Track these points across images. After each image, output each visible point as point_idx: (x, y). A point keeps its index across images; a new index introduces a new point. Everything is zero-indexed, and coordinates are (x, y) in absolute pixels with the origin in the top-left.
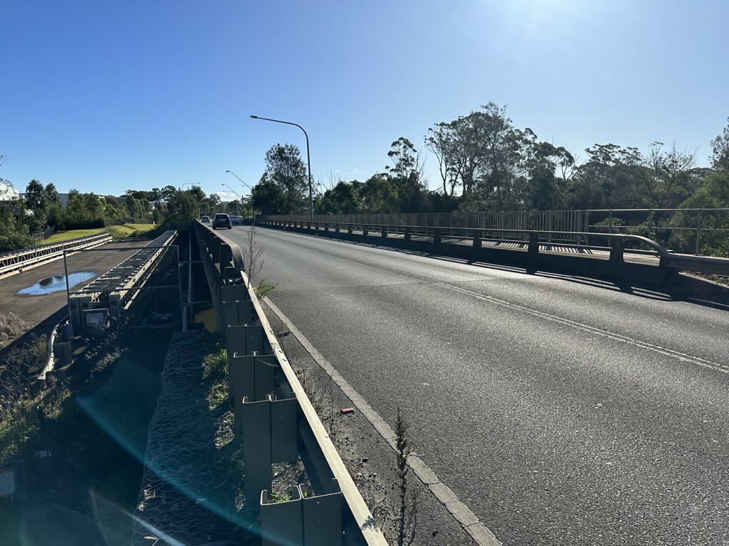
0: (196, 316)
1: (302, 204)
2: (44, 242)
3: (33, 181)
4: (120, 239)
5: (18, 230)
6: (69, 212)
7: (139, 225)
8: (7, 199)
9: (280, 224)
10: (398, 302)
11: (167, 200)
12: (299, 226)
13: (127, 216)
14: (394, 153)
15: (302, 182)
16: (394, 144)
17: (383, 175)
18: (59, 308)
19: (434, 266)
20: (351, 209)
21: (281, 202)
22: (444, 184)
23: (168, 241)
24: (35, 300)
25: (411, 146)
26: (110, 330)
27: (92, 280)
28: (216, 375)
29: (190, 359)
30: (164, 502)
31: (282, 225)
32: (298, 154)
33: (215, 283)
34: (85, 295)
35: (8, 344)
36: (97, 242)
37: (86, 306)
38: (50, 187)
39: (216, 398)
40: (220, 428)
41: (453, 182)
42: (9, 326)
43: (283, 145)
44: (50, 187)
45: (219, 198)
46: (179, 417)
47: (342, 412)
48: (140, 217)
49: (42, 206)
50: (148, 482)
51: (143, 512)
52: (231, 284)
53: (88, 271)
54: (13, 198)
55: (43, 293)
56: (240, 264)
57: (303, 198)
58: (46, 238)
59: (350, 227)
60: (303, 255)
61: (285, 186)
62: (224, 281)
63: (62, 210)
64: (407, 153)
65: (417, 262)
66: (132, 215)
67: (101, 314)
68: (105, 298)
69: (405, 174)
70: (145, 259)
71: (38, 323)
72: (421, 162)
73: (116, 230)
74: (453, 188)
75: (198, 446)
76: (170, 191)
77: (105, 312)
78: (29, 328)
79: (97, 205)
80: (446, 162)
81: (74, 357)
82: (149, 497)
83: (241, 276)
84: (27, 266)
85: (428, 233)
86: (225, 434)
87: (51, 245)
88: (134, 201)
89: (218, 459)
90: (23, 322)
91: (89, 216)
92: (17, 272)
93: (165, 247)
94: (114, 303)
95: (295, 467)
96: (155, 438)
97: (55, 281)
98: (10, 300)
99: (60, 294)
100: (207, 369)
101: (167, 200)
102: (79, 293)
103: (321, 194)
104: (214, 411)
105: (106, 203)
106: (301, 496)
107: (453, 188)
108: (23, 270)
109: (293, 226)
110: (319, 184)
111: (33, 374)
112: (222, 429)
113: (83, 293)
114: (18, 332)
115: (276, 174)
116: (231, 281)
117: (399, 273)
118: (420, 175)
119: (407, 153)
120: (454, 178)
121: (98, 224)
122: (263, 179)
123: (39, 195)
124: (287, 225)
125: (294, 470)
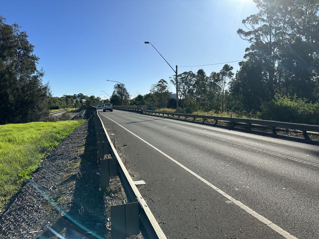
20: (143, 103)
25: (165, 82)
45: (100, 98)
66: (67, 105)
76: (81, 96)
106: (125, 203)
109: (130, 109)
121: (57, 108)
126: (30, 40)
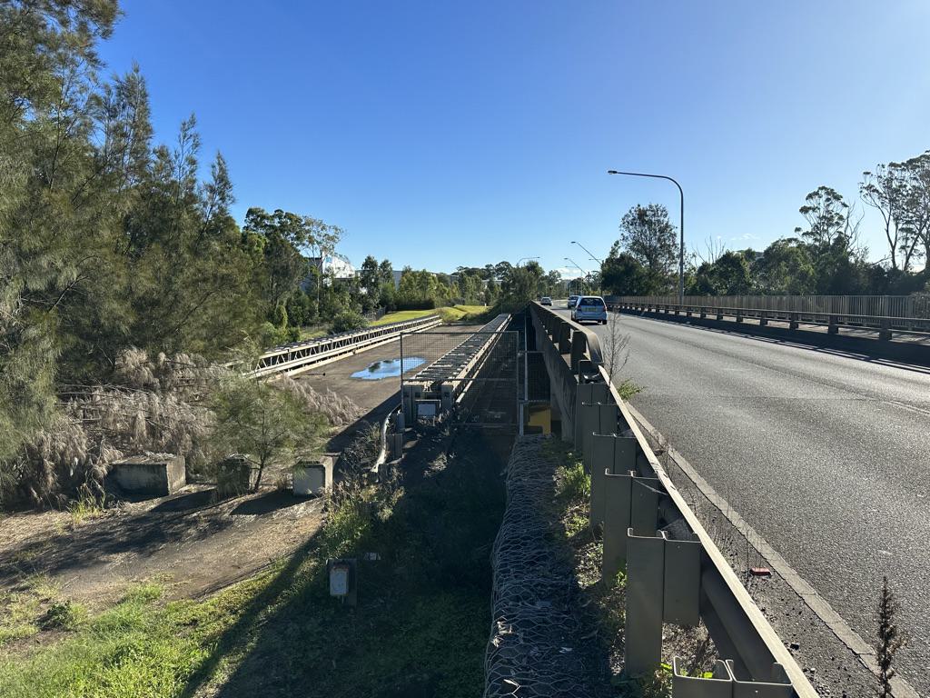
0: (531, 418)
1: (668, 282)
2: (376, 323)
3: (369, 258)
4: (450, 323)
5: (352, 307)
6: (401, 290)
7: (470, 307)
8: (344, 276)
9: (636, 308)
10: (827, 425)
11: (501, 278)
12: (663, 311)
13: (458, 296)
14: (810, 208)
15: (669, 252)
16: (810, 196)
17: (790, 240)
18: (390, 395)
19: (881, 375)
20: (741, 288)
21: (639, 279)
22: (893, 253)
23: (501, 326)
24: (366, 385)
25: (838, 198)
26: (441, 426)
27: (422, 367)
28: (572, 493)
29: (538, 470)
30: (522, 642)
31: (640, 309)
32: (666, 216)
33: (562, 379)
34: (418, 383)
35: (343, 429)
36: (427, 325)
37: (418, 396)
38: (385, 264)
39: (574, 523)
40: (582, 562)
41: (909, 250)
42: (344, 411)
43: (644, 206)
44: (385, 264)
45: (559, 275)
46: (529, 538)
47: (751, 571)
48: (471, 298)
49: (375, 285)
50: (501, 613)
51: (499, 648)
52: (588, 381)
53: (418, 357)
54: (350, 275)
55: (375, 378)
56: (597, 356)
57: (670, 273)
58: (377, 319)
59: (739, 314)
60: (671, 349)
61: (645, 259)
62: (577, 377)
63: (394, 288)
64: (830, 208)
65: (850, 368)
67: (434, 406)
68: (437, 386)
69: (825, 238)
70: (478, 346)
71: (370, 410)
72: (853, 221)
73: (446, 312)
74: (908, 259)
75: (555, 580)
76: (503, 268)
77: (437, 404)
78: (362, 414)
79: (428, 283)
80: (897, 219)
81: (405, 450)
82: (504, 632)
83: (598, 371)
84: (360, 348)
85: (849, 324)
86: (588, 570)
87: (383, 326)
88: (466, 277)
89: (583, 601)
90: (356, 408)
91: (420, 295)
92: (351, 354)
93: (499, 333)
94: (447, 394)
95: (690, 634)
96: (505, 560)
97: (383, 366)
98: (345, 382)
99: (390, 381)
100: (560, 483)
101: (501, 278)
102: (412, 381)
103: (694, 269)
104: (573, 539)
105: (437, 281)
107: (908, 259)
108: (357, 352)
109: (654, 310)
110: (694, 256)
111: (366, 464)
112: (585, 564)
113: (415, 380)
114: (353, 419)
115: (634, 244)
116: (586, 377)
117: (804, 377)
118: (851, 241)
119: (830, 208)
120: (910, 243)
121: (428, 305)
122: (613, 253)
123: (373, 272)
124: (646, 310)
125: (689, 637)
126: (149, 89)
